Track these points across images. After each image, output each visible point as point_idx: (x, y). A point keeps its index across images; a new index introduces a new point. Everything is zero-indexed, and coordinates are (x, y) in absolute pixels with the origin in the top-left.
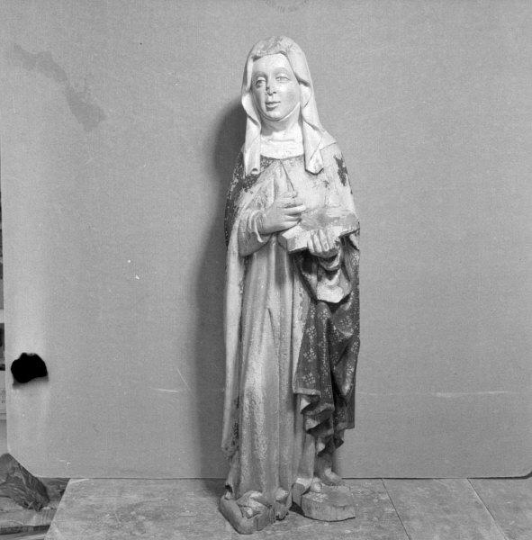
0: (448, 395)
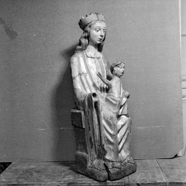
0: (142, 128)
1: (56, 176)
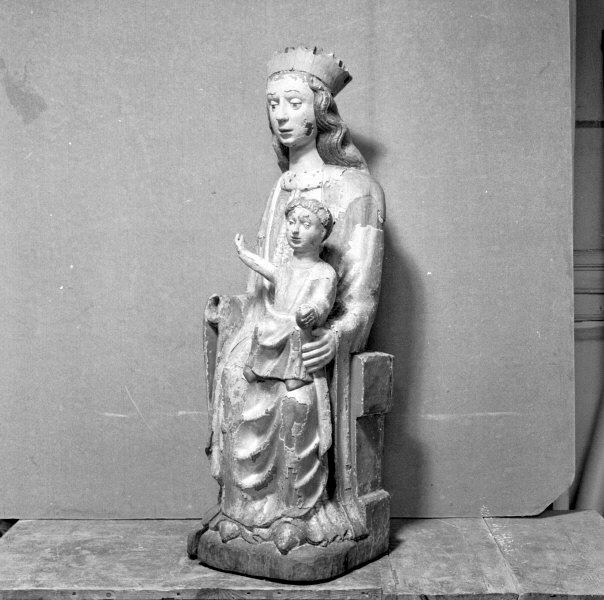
0: (442, 417)
1: (159, 568)
